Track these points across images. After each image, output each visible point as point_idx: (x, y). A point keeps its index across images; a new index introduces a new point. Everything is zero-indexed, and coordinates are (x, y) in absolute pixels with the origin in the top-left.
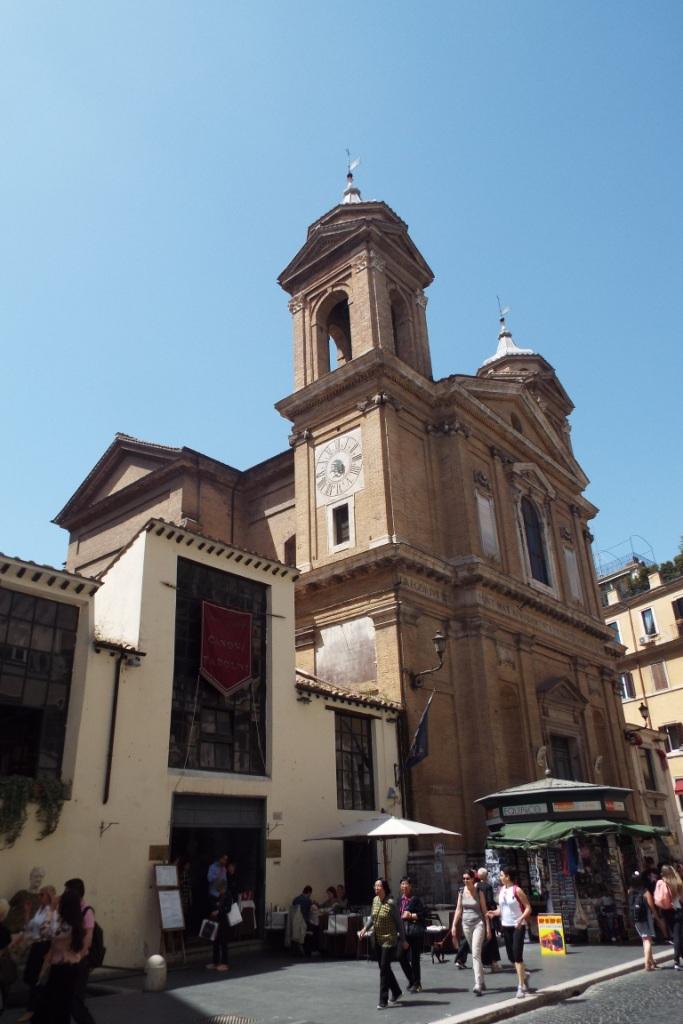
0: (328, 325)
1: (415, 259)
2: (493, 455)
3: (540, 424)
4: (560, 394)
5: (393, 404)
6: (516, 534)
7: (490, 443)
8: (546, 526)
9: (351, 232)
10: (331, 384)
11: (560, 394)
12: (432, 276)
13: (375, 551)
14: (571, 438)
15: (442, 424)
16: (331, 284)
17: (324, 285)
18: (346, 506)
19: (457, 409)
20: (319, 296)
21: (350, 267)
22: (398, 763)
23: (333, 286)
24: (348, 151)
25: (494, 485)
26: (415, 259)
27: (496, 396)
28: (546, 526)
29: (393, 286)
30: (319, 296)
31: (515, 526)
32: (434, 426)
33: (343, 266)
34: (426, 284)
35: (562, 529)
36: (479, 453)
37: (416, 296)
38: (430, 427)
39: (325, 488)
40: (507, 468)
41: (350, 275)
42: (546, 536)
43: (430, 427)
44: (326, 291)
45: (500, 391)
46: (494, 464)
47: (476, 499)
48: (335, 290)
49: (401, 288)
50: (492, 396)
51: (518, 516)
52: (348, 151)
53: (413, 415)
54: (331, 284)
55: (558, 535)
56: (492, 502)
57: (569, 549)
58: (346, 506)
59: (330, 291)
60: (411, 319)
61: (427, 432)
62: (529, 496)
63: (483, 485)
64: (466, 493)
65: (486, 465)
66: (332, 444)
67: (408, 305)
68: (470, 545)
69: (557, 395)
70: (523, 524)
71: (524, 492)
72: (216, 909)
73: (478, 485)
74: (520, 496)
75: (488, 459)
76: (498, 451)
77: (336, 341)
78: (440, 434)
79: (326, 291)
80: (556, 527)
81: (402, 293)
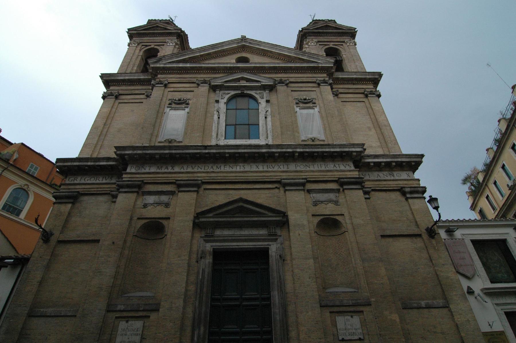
9: (344, 29)
10: (25, 256)
16: (156, 44)
17: (152, 42)
18: (475, 243)
20: (147, 46)
21: (344, 42)
23: (155, 45)
24: (67, 330)
30: (147, 46)
33: (342, 40)
41: (163, 45)
44: (150, 45)
52: (67, 330)
54: (156, 44)
58: (475, 243)
59: (152, 46)
66: (24, 318)
72: (150, 72)
77: (147, 222)
79: (150, 45)
81: (156, 47)
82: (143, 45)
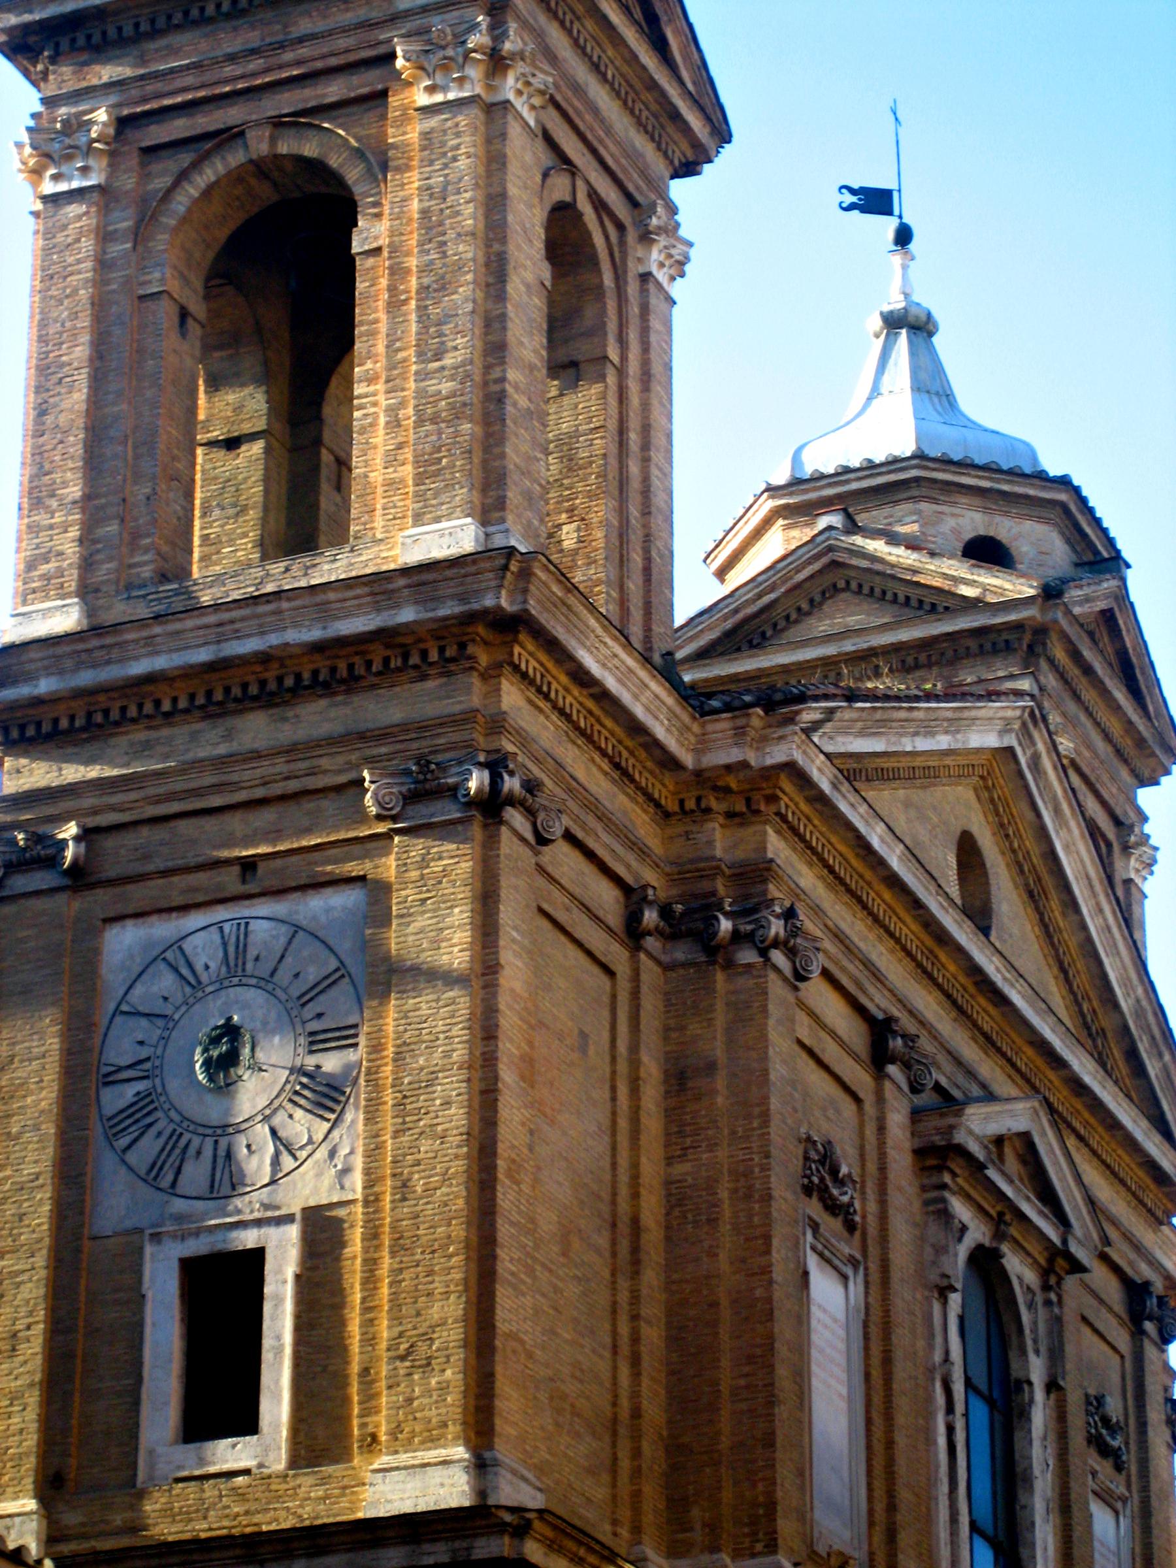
0: (209, 295)
1: (660, 46)
2: (879, 1058)
3: (1066, 887)
4: (1136, 693)
5: (531, 813)
6: (931, 1441)
7: (878, 1002)
8: (1039, 1395)
11: (1136, 693)
12: (723, 135)
13: (580, 1517)
14: (680, 317)
15: (707, 908)
19: (777, 847)
22: (1015, 1420)
23: (278, 123)
25: (872, 1207)
26: (660, 46)
27: (918, 762)
28: (1039, 1395)
29: (560, 188)
31: (930, 1399)
32: (665, 911)
34: (688, 169)
35: (1095, 1403)
36: (831, 1052)
37: (646, 238)
38: (650, 917)
39: (149, 1147)
40: (932, 1123)
42: (1037, 1451)
43: (650, 917)
44: (230, 136)
45: (943, 742)
46: (880, 1099)
47: (806, 1274)
48: (283, 148)
49: (600, 205)
50: (905, 762)
51: (946, 1359)
53: (590, 855)
55: (1077, 1439)
56: (856, 1287)
57: (1106, 1497)
60: (613, 354)
61: (633, 933)
62: (995, 1255)
63: (833, 1207)
64: (779, 1253)
65: (848, 1107)
67: (608, 279)
68: (771, 1506)
69: (1120, 695)
70: (959, 1388)
71: (978, 1233)
73: (814, 1208)
74: (963, 1251)
75: (859, 1076)
76: (531, 786)
78: (681, 952)
79: (230, 136)
80: (1074, 1399)
82: (151, 152)
